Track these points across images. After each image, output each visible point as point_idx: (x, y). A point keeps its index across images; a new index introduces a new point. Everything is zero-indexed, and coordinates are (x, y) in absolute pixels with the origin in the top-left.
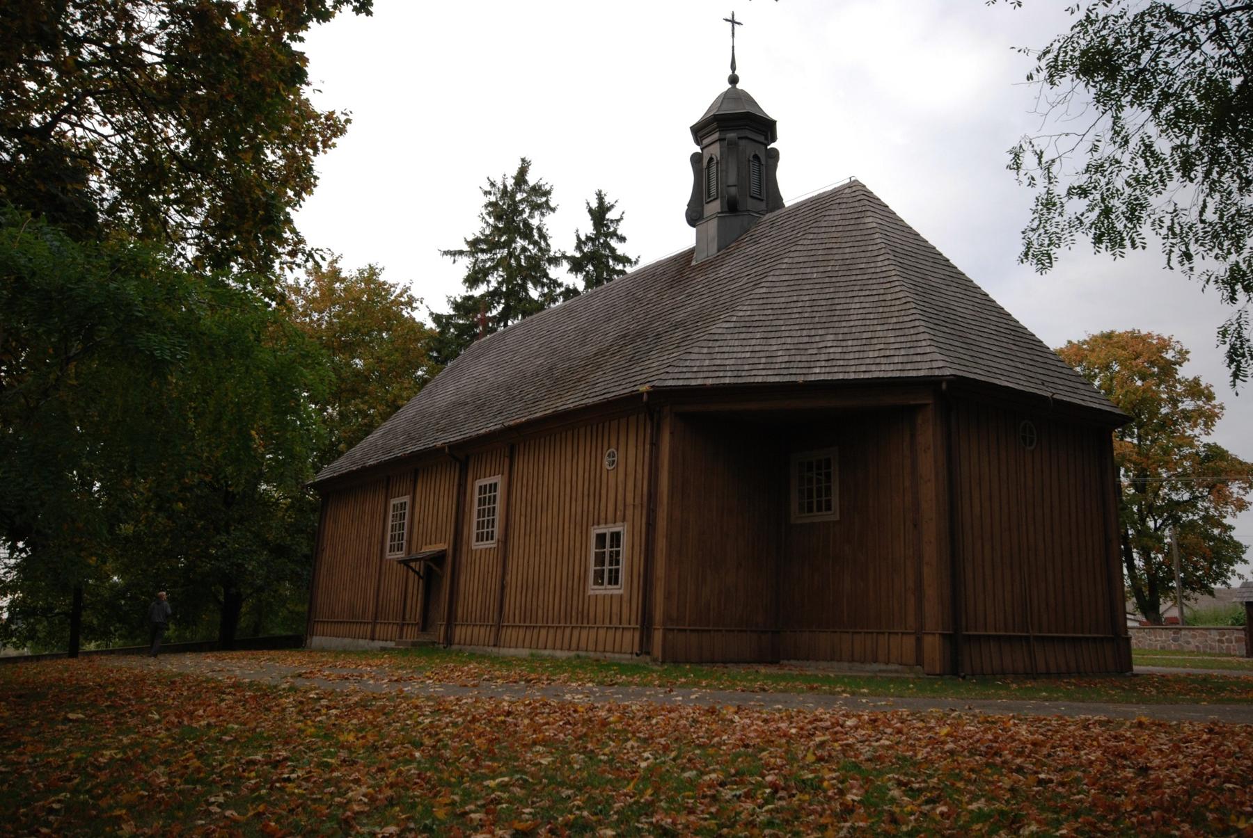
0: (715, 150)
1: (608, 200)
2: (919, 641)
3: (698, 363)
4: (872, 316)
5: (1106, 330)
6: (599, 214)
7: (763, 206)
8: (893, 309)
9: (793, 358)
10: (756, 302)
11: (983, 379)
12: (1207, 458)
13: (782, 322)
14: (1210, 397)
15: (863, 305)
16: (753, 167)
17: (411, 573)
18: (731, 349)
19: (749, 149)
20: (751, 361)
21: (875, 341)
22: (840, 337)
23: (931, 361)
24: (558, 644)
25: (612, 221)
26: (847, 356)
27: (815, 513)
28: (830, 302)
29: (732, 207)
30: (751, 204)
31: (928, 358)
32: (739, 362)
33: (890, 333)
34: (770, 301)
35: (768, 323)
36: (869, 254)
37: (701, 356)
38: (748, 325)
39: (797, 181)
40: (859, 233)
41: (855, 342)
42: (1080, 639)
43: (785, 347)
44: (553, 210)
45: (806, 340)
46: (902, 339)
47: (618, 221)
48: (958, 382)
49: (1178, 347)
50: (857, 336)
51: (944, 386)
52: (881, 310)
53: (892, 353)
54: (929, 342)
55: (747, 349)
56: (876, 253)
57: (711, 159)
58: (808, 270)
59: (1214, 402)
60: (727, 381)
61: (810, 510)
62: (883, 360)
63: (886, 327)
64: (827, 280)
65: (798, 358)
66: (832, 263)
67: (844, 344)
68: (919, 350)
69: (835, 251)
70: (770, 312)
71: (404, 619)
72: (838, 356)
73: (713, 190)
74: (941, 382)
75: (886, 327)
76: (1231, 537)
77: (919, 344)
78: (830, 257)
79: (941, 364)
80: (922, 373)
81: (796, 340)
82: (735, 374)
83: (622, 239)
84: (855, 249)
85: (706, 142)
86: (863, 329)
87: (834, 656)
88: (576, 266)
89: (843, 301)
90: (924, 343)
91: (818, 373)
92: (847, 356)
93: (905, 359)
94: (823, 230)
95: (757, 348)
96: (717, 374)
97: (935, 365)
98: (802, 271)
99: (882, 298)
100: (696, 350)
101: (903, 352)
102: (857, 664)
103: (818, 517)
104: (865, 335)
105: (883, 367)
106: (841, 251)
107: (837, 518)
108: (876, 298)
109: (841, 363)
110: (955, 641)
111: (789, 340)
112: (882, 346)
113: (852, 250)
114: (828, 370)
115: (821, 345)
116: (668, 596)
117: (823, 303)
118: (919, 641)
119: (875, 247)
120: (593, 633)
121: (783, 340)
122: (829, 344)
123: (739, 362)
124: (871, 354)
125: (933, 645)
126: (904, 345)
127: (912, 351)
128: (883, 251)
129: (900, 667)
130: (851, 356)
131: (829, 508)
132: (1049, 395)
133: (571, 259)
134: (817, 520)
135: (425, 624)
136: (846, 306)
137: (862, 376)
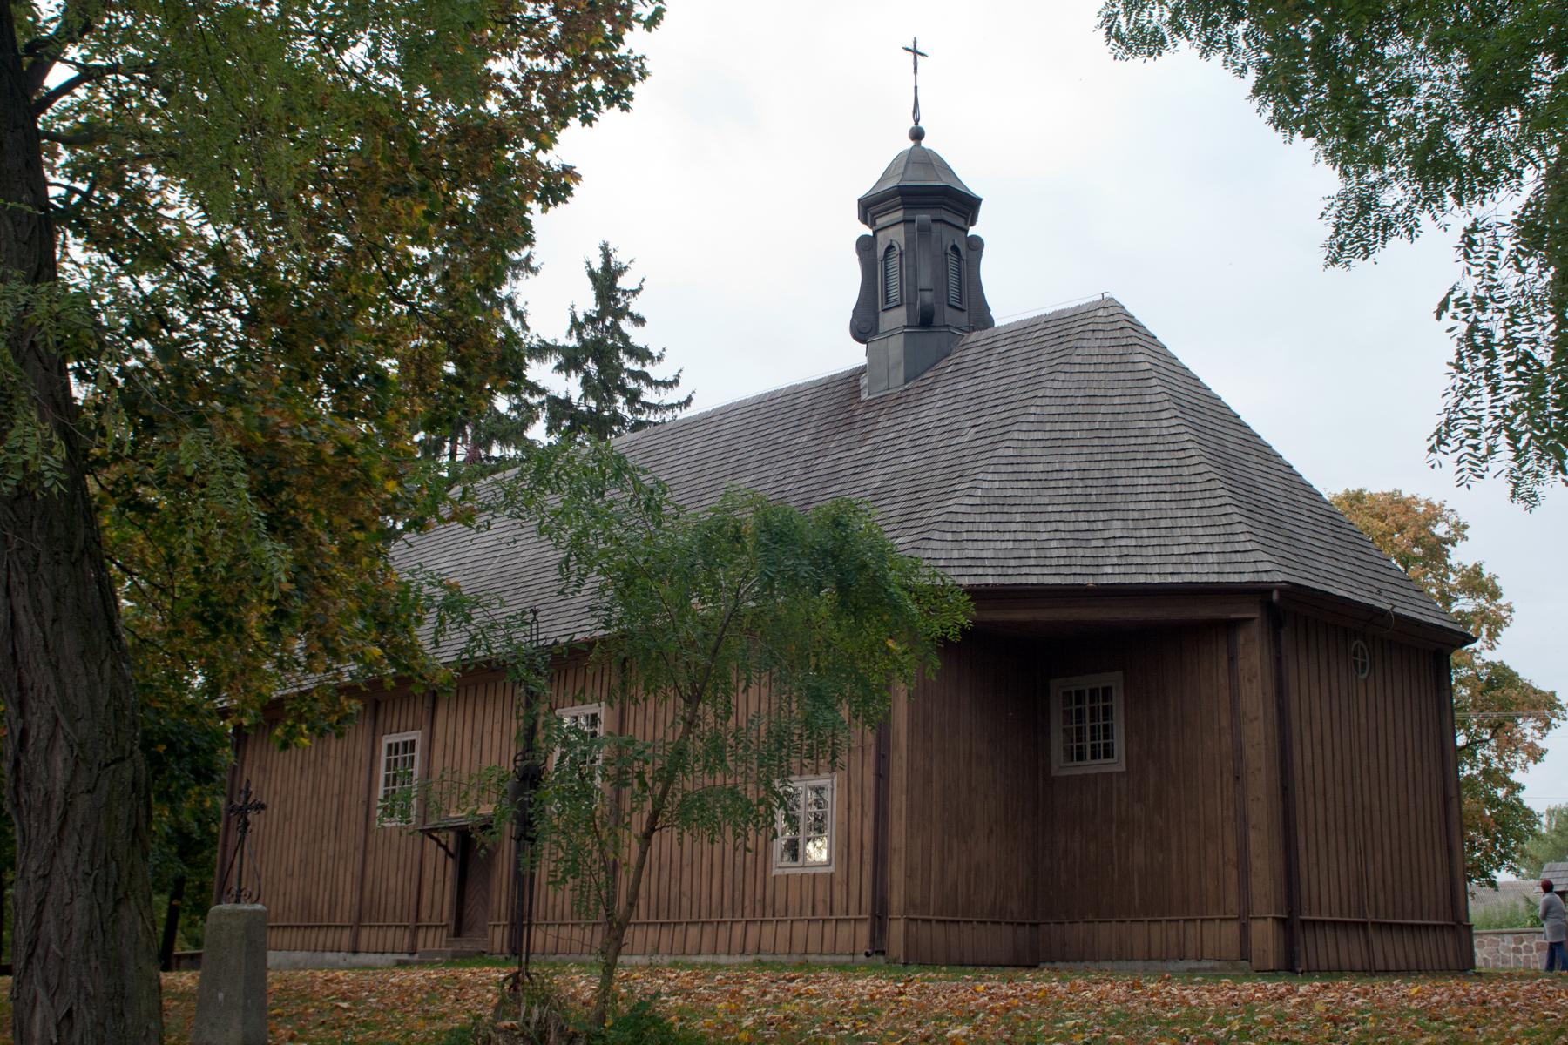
0: (898, 235)
1: (618, 258)
2: (1244, 929)
3: (943, 554)
4: (1167, 497)
5: (1354, 488)
6: (606, 280)
7: (963, 318)
8: (1194, 488)
9: (1072, 552)
10: (1003, 469)
11: (1317, 586)
12: (1490, 684)
13: (1046, 500)
14: (1495, 594)
15: (1153, 481)
16: (952, 258)
17: (441, 850)
18: (986, 536)
19: (948, 237)
20: (1016, 554)
21: (1178, 532)
22: (1131, 525)
23: (1254, 564)
24: (722, 945)
25: (624, 292)
26: (1144, 552)
27: (1089, 761)
28: (1106, 474)
29: (925, 320)
30: (950, 316)
31: (1250, 557)
32: (1001, 554)
33: (1196, 522)
34: (1022, 468)
35: (1027, 501)
36: (1147, 408)
37: (944, 545)
38: (1000, 503)
39: (1020, 280)
40: (1129, 376)
41: (1152, 533)
42: (1419, 926)
43: (1058, 535)
44: (535, 271)
45: (1085, 526)
46: (1214, 530)
47: (635, 292)
48: (1293, 592)
49: (1453, 519)
50: (1153, 523)
51: (1275, 596)
52: (1178, 488)
53: (1203, 549)
54: (1249, 537)
55: (1007, 536)
56: (1157, 407)
57: (890, 248)
58: (1068, 427)
59: (1500, 601)
60: (990, 581)
61: (1081, 757)
62: (1194, 559)
63: (1188, 513)
64: (1096, 442)
65: (1080, 552)
66: (1099, 417)
67: (1137, 534)
68: (1237, 547)
69: (1099, 401)
70: (1026, 484)
71: (417, 918)
72: (1132, 551)
73: (895, 293)
74: (1270, 591)
75: (1188, 513)
76: (1518, 800)
77: (1236, 538)
78: (1095, 409)
79: (1268, 567)
80: (1246, 578)
81: (1071, 527)
82: (999, 571)
83: (639, 320)
84: (1127, 400)
85: (881, 221)
86: (1159, 514)
87: (1122, 954)
88: (570, 361)
89: (1123, 473)
90: (1242, 538)
91: (1110, 575)
92: (1144, 552)
93: (1221, 558)
94: (1077, 368)
95: (1021, 536)
96: (974, 571)
97: (1261, 567)
98: (1058, 426)
99: (1176, 471)
100: (936, 535)
101: (1217, 548)
102: (1157, 963)
103: (1091, 767)
104: (1163, 523)
105: (1195, 568)
106: (1107, 401)
107: (1123, 768)
108: (1169, 472)
109: (1139, 560)
110: (1290, 925)
111: (1061, 526)
112: (1188, 540)
113: (1123, 400)
114: (1122, 569)
115: (1107, 534)
116: (910, 876)
117: (1097, 474)
118: (1244, 929)
119: (1154, 399)
120: (784, 930)
121: (1054, 526)
122: (1118, 534)
123: (1001, 554)
124: (1176, 550)
125: (1265, 934)
126: (1217, 539)
127: (1229, 548)
128: (1166, 405)
129: (1217, 964)
130: (1150, 551)
131: (1108, 754)
132: (1389, 607)
133: (563, 350)
134: (1092, 771)
135: (460, 926)
136: (1129, 481)
137: (1170, 579)
